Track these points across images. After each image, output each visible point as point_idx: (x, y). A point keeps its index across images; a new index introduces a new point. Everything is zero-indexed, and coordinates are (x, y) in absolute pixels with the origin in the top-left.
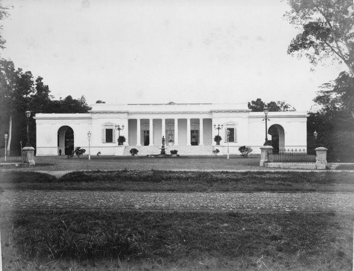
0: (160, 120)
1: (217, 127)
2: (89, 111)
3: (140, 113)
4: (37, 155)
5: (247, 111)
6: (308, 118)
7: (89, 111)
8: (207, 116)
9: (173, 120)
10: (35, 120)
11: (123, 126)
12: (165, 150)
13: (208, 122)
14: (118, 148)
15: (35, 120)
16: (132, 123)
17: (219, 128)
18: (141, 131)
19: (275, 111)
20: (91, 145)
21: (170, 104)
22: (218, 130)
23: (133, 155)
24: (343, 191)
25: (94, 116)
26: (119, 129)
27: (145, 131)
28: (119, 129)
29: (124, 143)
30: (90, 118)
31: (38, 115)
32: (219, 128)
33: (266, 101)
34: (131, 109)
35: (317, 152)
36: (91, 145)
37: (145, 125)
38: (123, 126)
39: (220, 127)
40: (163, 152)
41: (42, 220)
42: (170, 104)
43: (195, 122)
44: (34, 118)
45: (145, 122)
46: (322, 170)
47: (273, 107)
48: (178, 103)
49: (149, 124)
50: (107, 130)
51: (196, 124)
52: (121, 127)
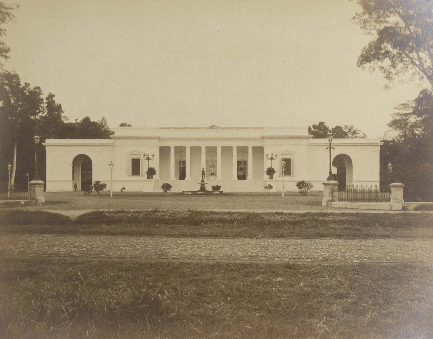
0: (231, 148)
1: (270, 156)
2: (111, 136)
3: (174, 139)
4: (47, 190)
5: (307, 138)
8: (257, 144)
10: (45, 147)
11: (153, 155)
13: (259, 151)
15: (45, 147)
16: (164, 151)
17: (272, 159)
18: (176, 161)
21: (212, 127)
22: (147, 161)
25: (117, 142)
26: (148, 159)
27: (180, 162)
28: (148, 159)
29: (154, 176)
30: (113, 145)
31: (49, 142)
32: (272, 159)
33: (331, 125)
34: (163, 134)
35: (392, 189)
38: (153, 155)
39: (274, 157)
40: (203, 188)
42: (212, 127)
44: (44, 144)
45: (180, 150)
49: (185, 152)
50: (133, 160)
52: (150, 156)
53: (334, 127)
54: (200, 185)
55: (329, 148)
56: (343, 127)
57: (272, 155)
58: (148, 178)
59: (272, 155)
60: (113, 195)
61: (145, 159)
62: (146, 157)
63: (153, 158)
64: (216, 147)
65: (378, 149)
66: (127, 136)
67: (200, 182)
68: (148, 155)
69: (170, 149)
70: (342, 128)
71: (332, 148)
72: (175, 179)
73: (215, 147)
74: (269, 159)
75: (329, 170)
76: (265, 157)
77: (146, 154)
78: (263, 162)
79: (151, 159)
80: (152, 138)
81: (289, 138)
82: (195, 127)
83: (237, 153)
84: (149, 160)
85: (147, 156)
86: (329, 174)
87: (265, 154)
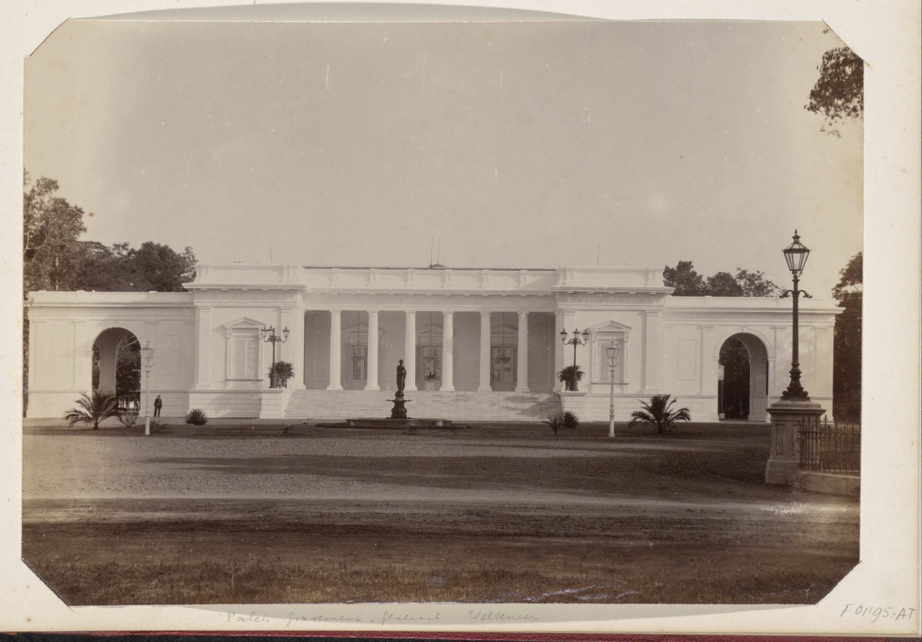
0: (514, 316)
1: (571, 336)
2: (185, 285)
4: (28, 416)
6: (837, 316)
7: (185, 285)
8: (539, 307)
9: (514, 316)
11: (286, 331)
12: (406, 405)
13: (544, 325)
14: (272, 396)
16: (316, 323)
17: (575, 342)
19: (730, 294)
20: (610, 386)
21: (431, 267)
22: (270, 344)
23: (768, 410)
24: (76, 503)
28: (273, 339)
29: (290, 381)
33: (705, 270)
34: (314, 282)
36: (610, 386)
37: (356, 329)
38: (286, 331)
39: (581, 338)
41: (579, 583)
42: (431, 267)
43: (505, 323)
46: (528, 447)
47: (723, 285)
48: (457, 266)
49: (367, 325)
51: (507, 330)
53: (712, 274)
54: (393, 405)
55: (790, 294)
56: (734, 274)
57: (576, 333)
58: (272, 386)
59: (576, 333)
60: (615, 431)
61: (266, 339)
62: (268, 335)
63: (286, 337)
64: (403, 312)
65: (832, 320)
66: (614, 289)
67: (394, 398)
68: (273, 330)
69: (330, 317)
70: (701, 276)
71: (802, 295)
72: (340, 388)
73: (512, 313)
74: (570, 342)
75: (791, 367)
76: (558, 336)
77: (268, 328)
78: (479, 346)
79: (580, 343)
80: (244, 289)
81: (616, 293)
82: (318, 265)
83: (492, 328)
84: (577, 346)
85: (271, 332)
86: (790, 379)
87: (558, 330)
